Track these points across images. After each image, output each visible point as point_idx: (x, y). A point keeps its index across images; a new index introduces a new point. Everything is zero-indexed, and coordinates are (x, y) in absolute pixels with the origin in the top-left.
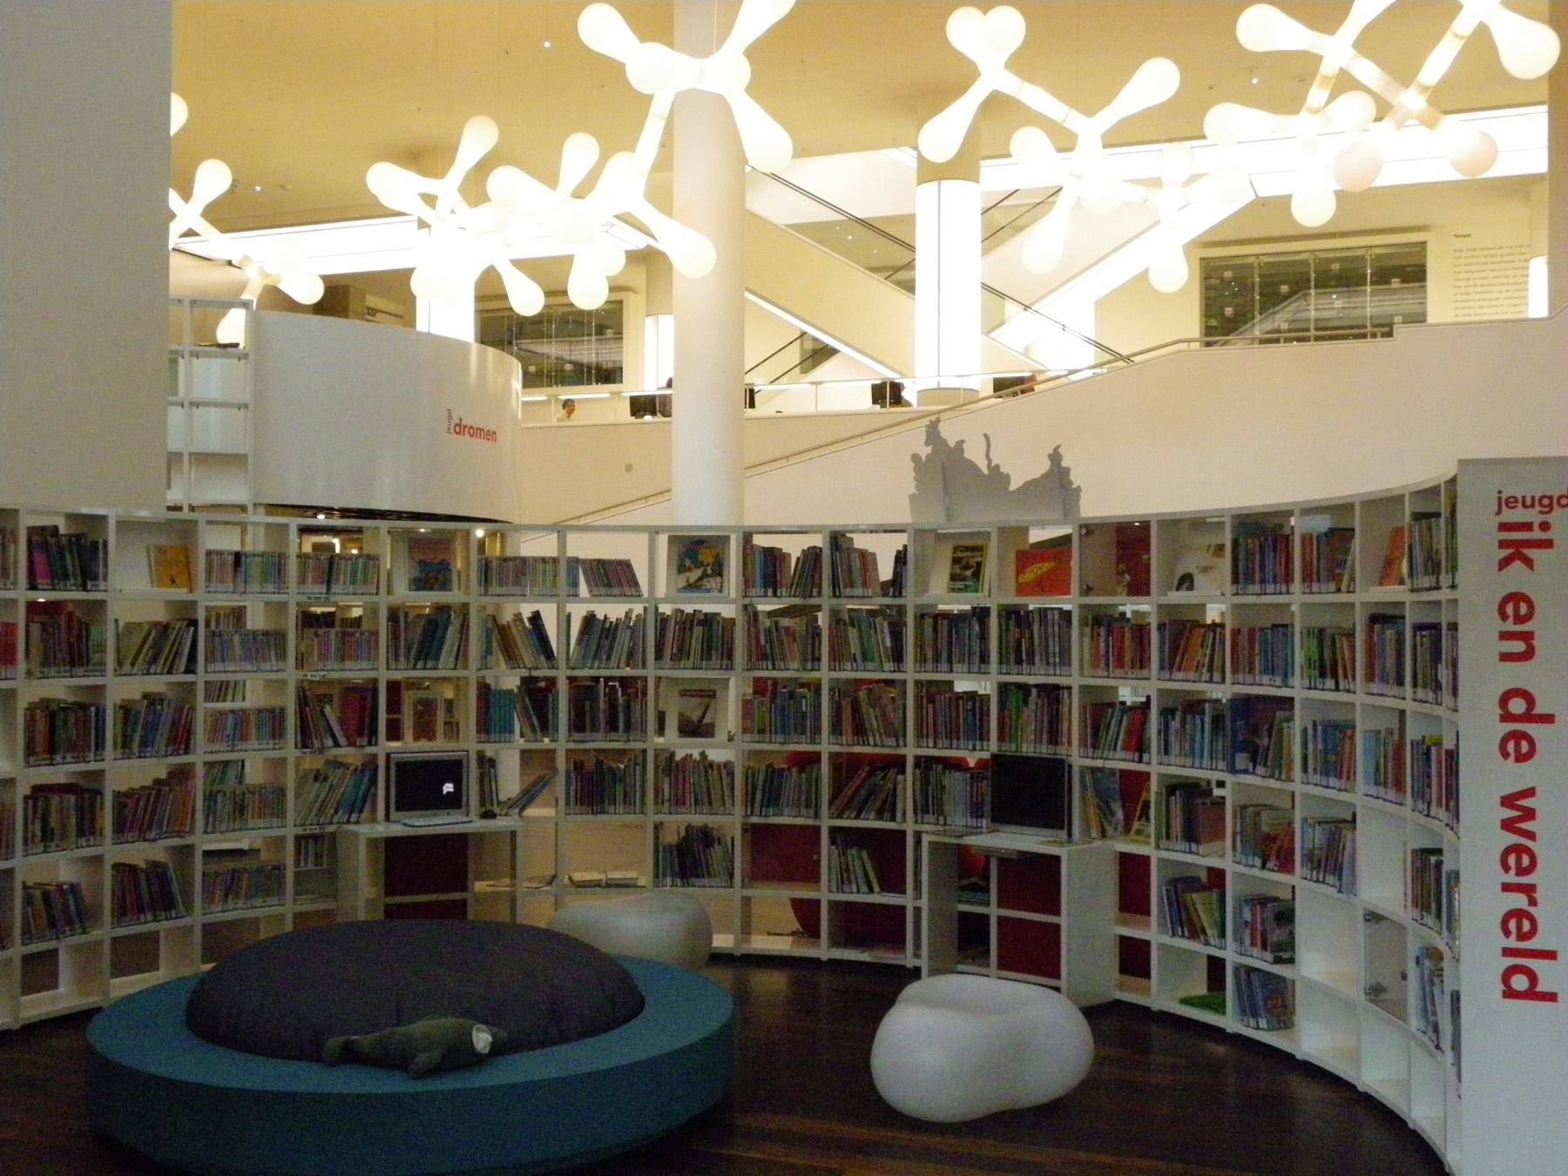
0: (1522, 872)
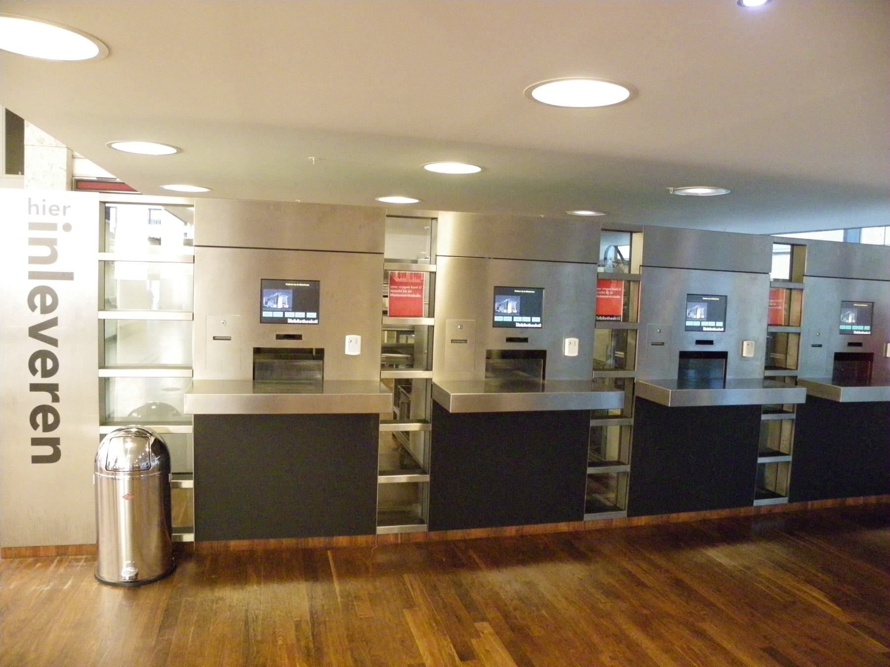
0: (47, 428)
